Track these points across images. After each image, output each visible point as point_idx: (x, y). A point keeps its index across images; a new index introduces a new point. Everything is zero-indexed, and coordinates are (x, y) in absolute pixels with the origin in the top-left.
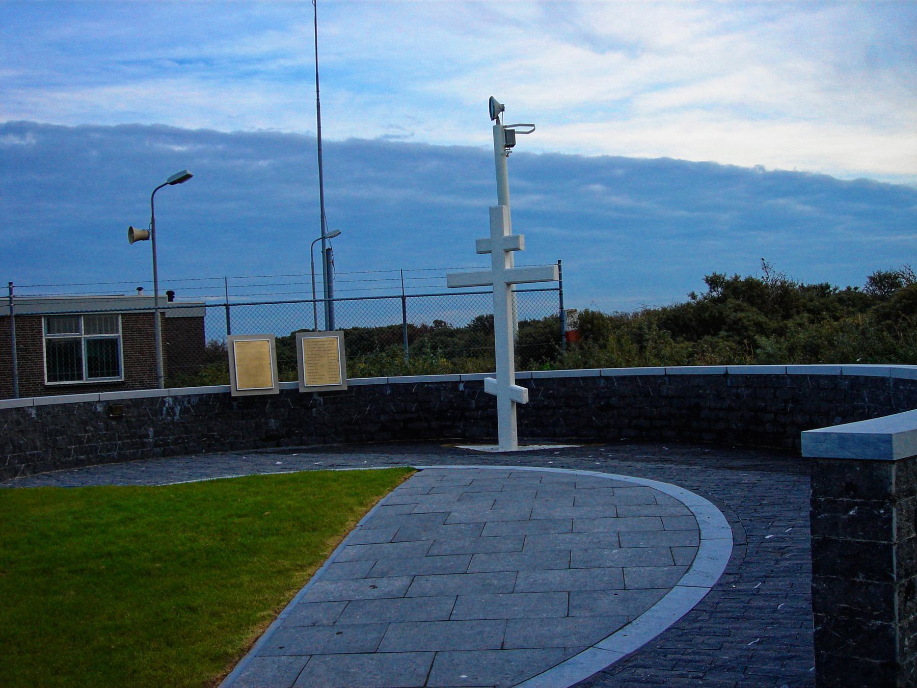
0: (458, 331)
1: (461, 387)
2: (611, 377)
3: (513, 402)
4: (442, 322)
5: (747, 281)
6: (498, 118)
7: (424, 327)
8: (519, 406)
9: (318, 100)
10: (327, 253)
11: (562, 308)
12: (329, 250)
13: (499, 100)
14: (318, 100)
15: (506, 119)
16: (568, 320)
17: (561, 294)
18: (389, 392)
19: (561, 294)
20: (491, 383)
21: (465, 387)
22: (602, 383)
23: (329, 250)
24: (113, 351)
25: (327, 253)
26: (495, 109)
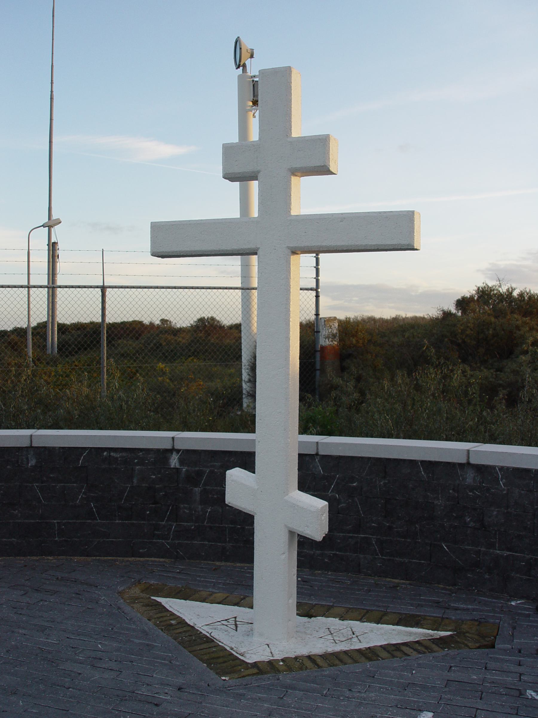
0: (181, 330)
1: (174, 461)
2: (493, 467)
3: (291, 533)
4: (167, 321)
5: (521, 295)
6: (244, 66)
7: (152, 324)
8: (304, 544)
9: (52, 92)
10: (53, 247)
11: (317, 315)
12: (55, 244)
13: (247, 43)
14: (52, 92)
15: (254, 68)
16: (324, 332)
17: (317, 296)
18: (33, 462)
19: (317, 296)
20: (240, 488)
21: (181, 461)
22: (470, 477)
23: (55, 244)
24: (52, 319)
25: (53, 247)
26: (240, 56)
